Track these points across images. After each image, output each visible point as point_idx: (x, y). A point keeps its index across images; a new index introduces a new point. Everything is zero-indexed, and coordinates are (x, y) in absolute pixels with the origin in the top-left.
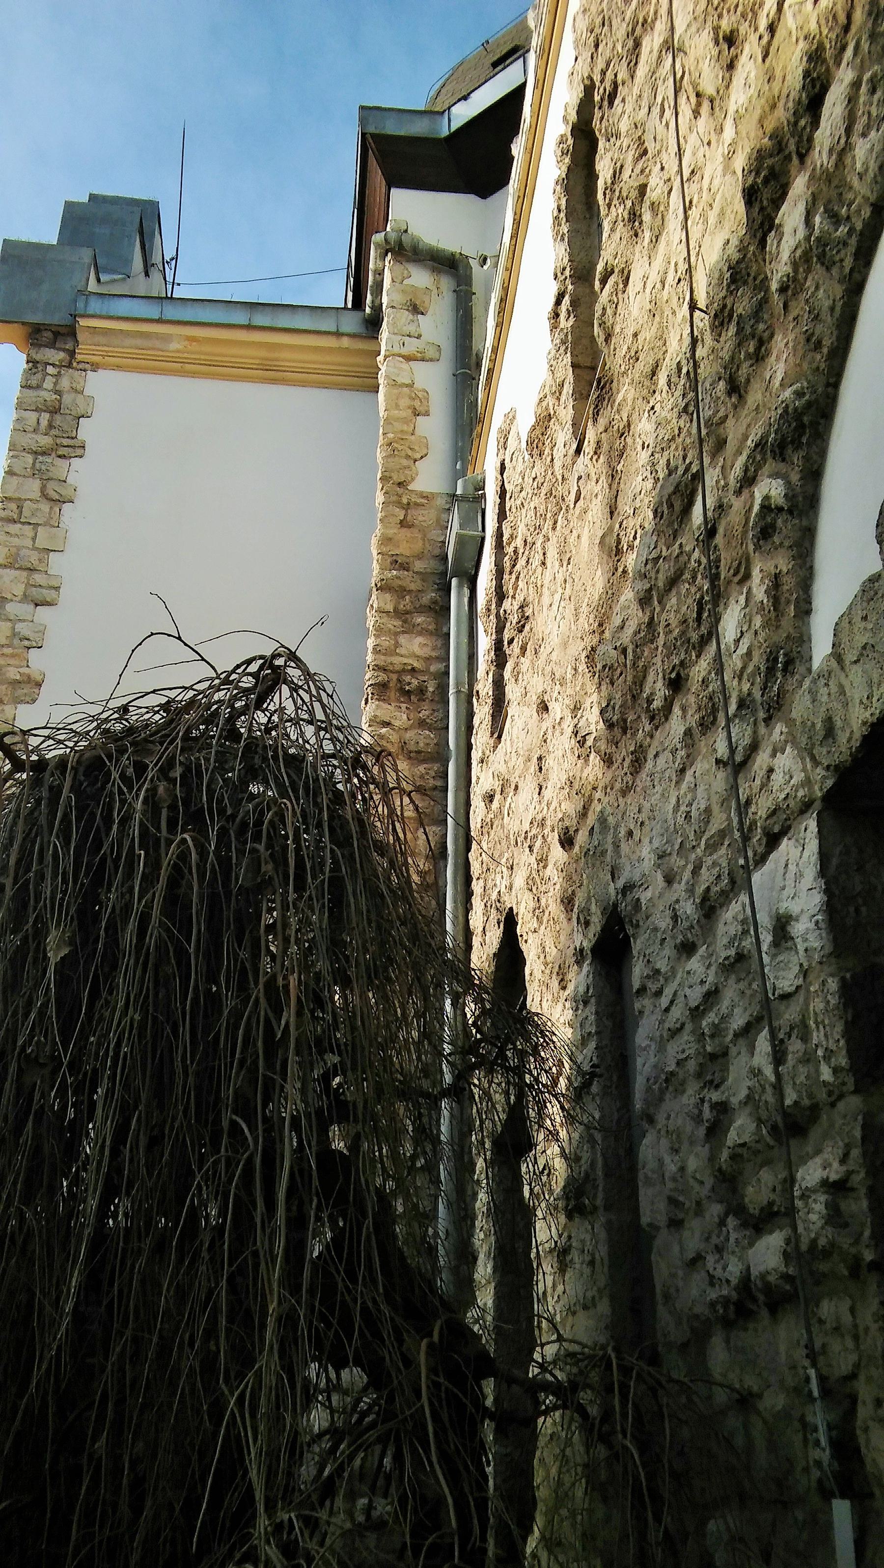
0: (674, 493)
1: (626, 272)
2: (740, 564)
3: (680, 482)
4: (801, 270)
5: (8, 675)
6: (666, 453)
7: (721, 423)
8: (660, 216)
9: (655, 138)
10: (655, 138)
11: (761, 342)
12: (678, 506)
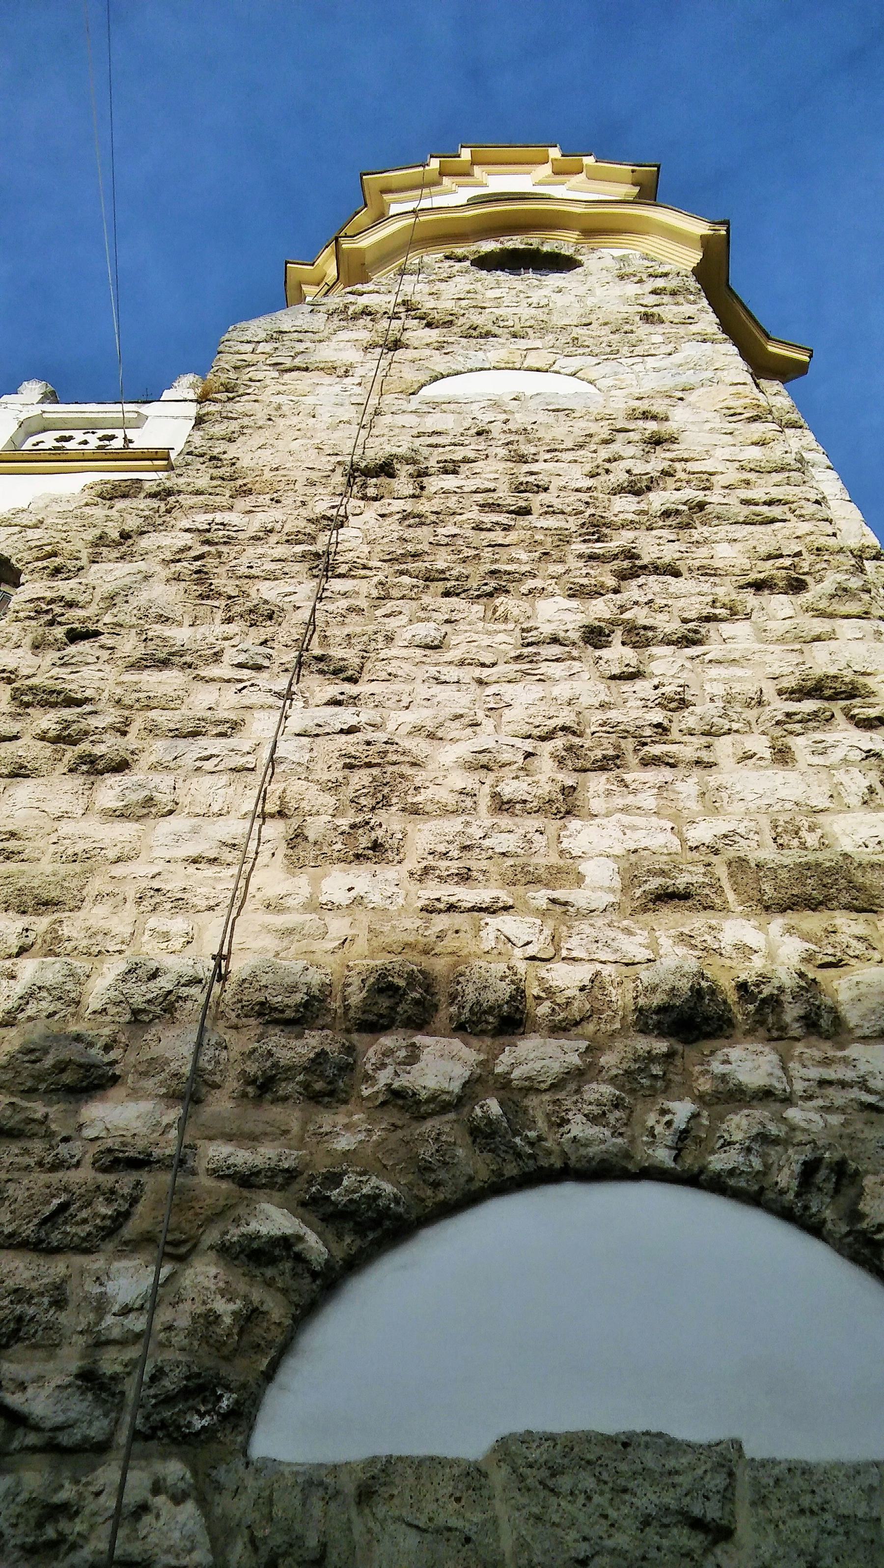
0: (80, 1066)
1: (23, 771)
2: (184, 1242)
3: (99, 1067)
4: (432, 1106)
5: (711, 1167)
6: (59, 1005)
7: (209, 1086)
8: (145, 811)
9: (176, 758)
10: (176, 758)
11: (331, 1093)
12: (67, 1078)
